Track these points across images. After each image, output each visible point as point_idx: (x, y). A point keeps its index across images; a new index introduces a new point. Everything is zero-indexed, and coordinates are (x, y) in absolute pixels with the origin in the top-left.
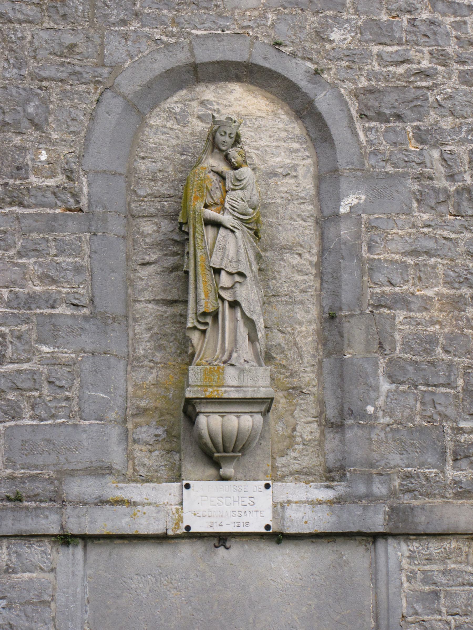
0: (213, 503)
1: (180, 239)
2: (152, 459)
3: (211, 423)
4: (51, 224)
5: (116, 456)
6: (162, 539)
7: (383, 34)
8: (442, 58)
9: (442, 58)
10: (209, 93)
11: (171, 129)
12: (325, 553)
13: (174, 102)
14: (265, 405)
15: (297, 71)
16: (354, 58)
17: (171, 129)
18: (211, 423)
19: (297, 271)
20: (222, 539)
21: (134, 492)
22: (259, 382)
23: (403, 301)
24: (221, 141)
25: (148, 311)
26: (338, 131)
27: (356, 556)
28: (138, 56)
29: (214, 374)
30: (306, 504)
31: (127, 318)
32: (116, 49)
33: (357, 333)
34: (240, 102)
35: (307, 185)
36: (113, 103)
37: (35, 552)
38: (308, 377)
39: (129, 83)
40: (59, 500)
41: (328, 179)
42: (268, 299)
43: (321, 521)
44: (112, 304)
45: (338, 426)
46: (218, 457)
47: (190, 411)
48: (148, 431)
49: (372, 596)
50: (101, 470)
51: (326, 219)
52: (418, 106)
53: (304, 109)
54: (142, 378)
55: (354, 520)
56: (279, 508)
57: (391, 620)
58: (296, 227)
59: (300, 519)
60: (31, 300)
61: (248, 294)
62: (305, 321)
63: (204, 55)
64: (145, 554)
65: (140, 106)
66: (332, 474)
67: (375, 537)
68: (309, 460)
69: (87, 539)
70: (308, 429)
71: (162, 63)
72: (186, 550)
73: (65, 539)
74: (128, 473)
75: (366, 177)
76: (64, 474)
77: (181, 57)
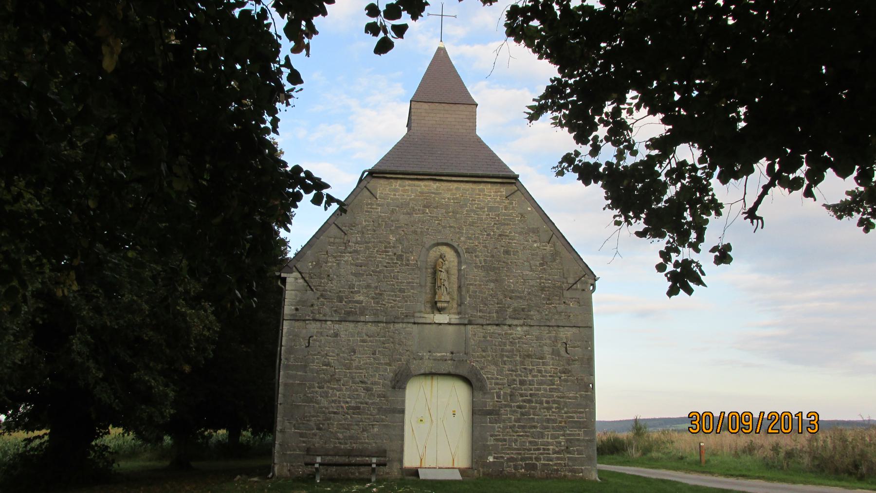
0: (440, 318)
1: (435, 273)
2: (429, 310)
3: (439, 305)
4: (413, 270)
5: (423, 310)
6: (430, 324)
7: (470, 238)
8: (479, 243)
9: (479, 243)
10: (440, 247)
11: (434, 253)
12: (457, 327)
13: (434, 249)
14: (448, 302)
15: (455, 245)
16: (465, 242)
17: (434, 253)
18: (439, 305)
19: (454, 278)
20: (440, 324)
21: (426, 315)
22: (447, 298)
23: (471, 284)
24: (442, 256)
25: (429, 284)
26: (462, 255)
27: (462, 327)
28: (429, 241)
29: (440, 297)
30: (455, 318)
31: (425, 286)
32: (425, 240)
33: (464, 289)
34: (445, 249)
35: (456, 264)
36: (424, 249)
37: (410, 325)
38: (455, 297)
39: (427, 246)
40: (413, 316)
41: (460, 263)
42: (449, 283)
43: (457, 321)
44: (423, 284)
45: (460, 305)
46: (440, 310)
47: (436, 303)
48: (429, 305)
49: (489, 327)
50: (420, 312)
51: (459, 270)
52: (475, 251)
53: (456, 251)
54: (426, 296)
55: (462, 321)
56: (450, 319)
57: (463, 280)
58: (454, 271)
59: (453, 321)
60: (410, 283)
61: (446, 283)
62: (455, 286)
63: (440, 241)
64: (428, 326)
65: (428, 250)
66: (459, 313)
67: (465, 325)
68: (455, 311)
69: (418, 323)
70: (455, 306)
71: (433, 242)
72: (434, 326)
73: (414, 323)
74: (186, 189)
75: (466, 263)
76: (414, 312)
77: (436, 242)
